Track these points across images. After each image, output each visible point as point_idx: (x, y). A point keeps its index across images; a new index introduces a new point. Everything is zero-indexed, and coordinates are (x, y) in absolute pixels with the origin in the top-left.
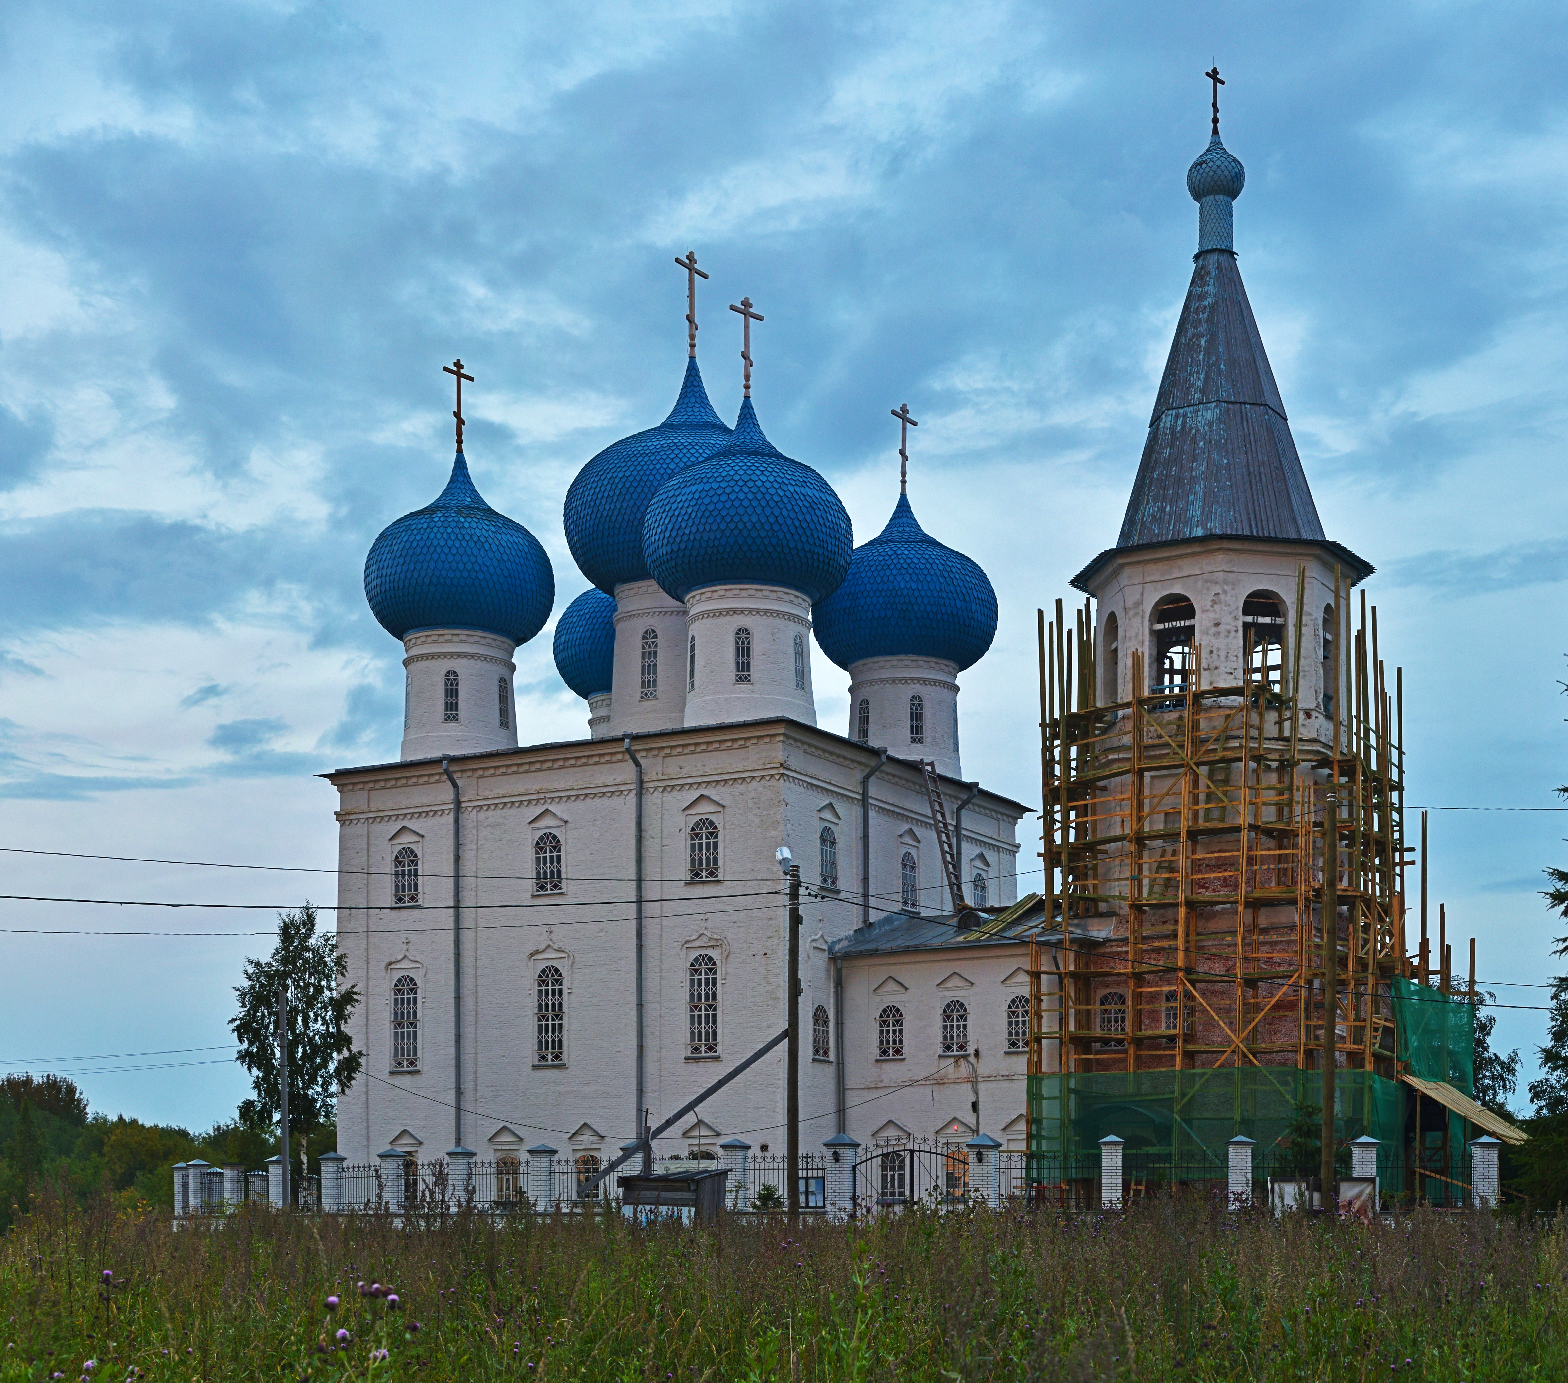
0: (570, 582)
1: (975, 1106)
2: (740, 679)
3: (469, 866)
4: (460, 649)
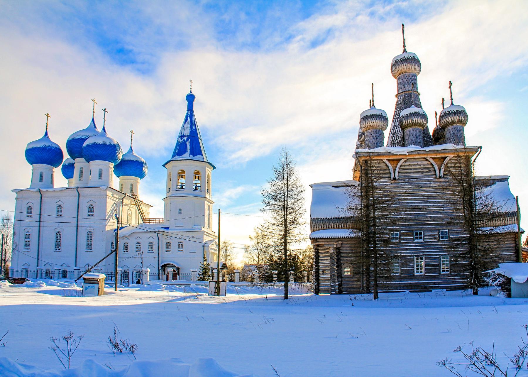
0: (66, 156)
1: (142, 263)
2: (99, 179)
3: (42, 213)
4: (42, 167)
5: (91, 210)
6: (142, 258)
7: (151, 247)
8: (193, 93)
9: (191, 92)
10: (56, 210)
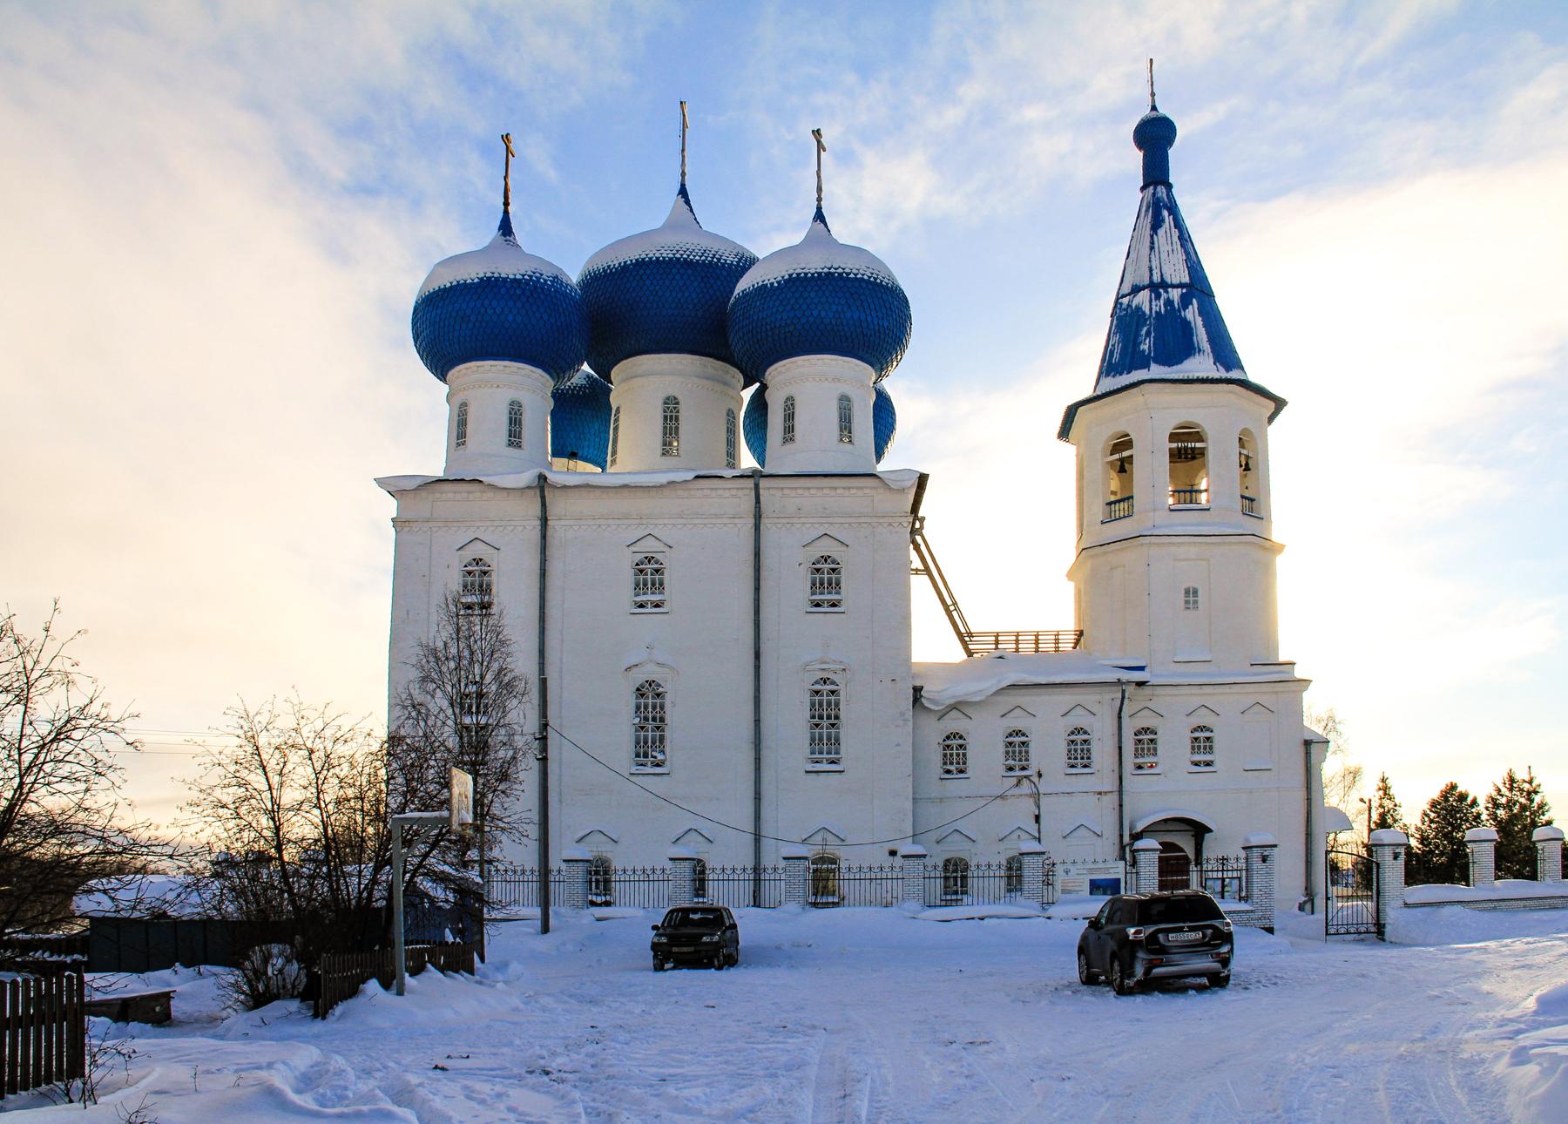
1: (1037, 818)
5: (826, 581)
6: (1036, 797)
7: (1079, 751)
8: (1163, 110)
9: (1154, 108)
10: (629, 577)
